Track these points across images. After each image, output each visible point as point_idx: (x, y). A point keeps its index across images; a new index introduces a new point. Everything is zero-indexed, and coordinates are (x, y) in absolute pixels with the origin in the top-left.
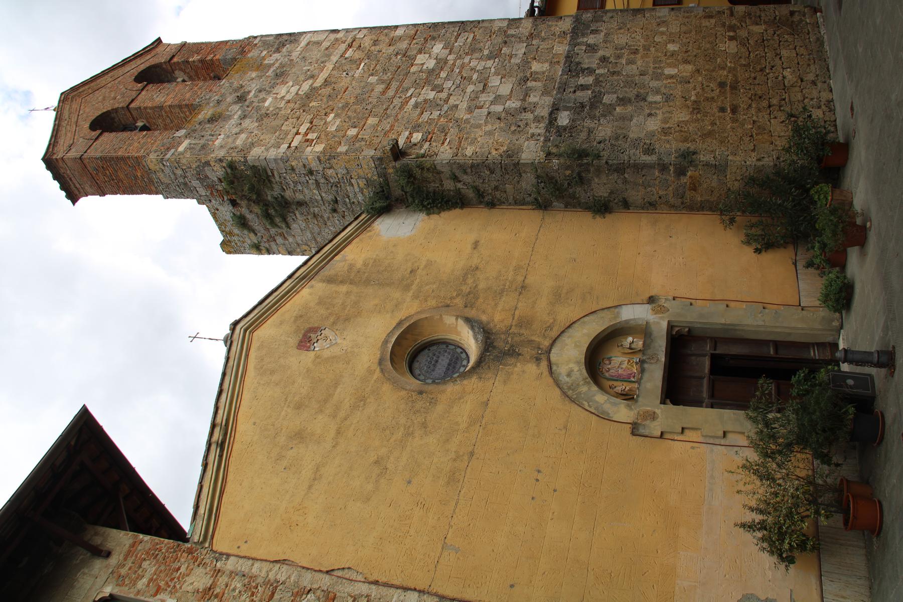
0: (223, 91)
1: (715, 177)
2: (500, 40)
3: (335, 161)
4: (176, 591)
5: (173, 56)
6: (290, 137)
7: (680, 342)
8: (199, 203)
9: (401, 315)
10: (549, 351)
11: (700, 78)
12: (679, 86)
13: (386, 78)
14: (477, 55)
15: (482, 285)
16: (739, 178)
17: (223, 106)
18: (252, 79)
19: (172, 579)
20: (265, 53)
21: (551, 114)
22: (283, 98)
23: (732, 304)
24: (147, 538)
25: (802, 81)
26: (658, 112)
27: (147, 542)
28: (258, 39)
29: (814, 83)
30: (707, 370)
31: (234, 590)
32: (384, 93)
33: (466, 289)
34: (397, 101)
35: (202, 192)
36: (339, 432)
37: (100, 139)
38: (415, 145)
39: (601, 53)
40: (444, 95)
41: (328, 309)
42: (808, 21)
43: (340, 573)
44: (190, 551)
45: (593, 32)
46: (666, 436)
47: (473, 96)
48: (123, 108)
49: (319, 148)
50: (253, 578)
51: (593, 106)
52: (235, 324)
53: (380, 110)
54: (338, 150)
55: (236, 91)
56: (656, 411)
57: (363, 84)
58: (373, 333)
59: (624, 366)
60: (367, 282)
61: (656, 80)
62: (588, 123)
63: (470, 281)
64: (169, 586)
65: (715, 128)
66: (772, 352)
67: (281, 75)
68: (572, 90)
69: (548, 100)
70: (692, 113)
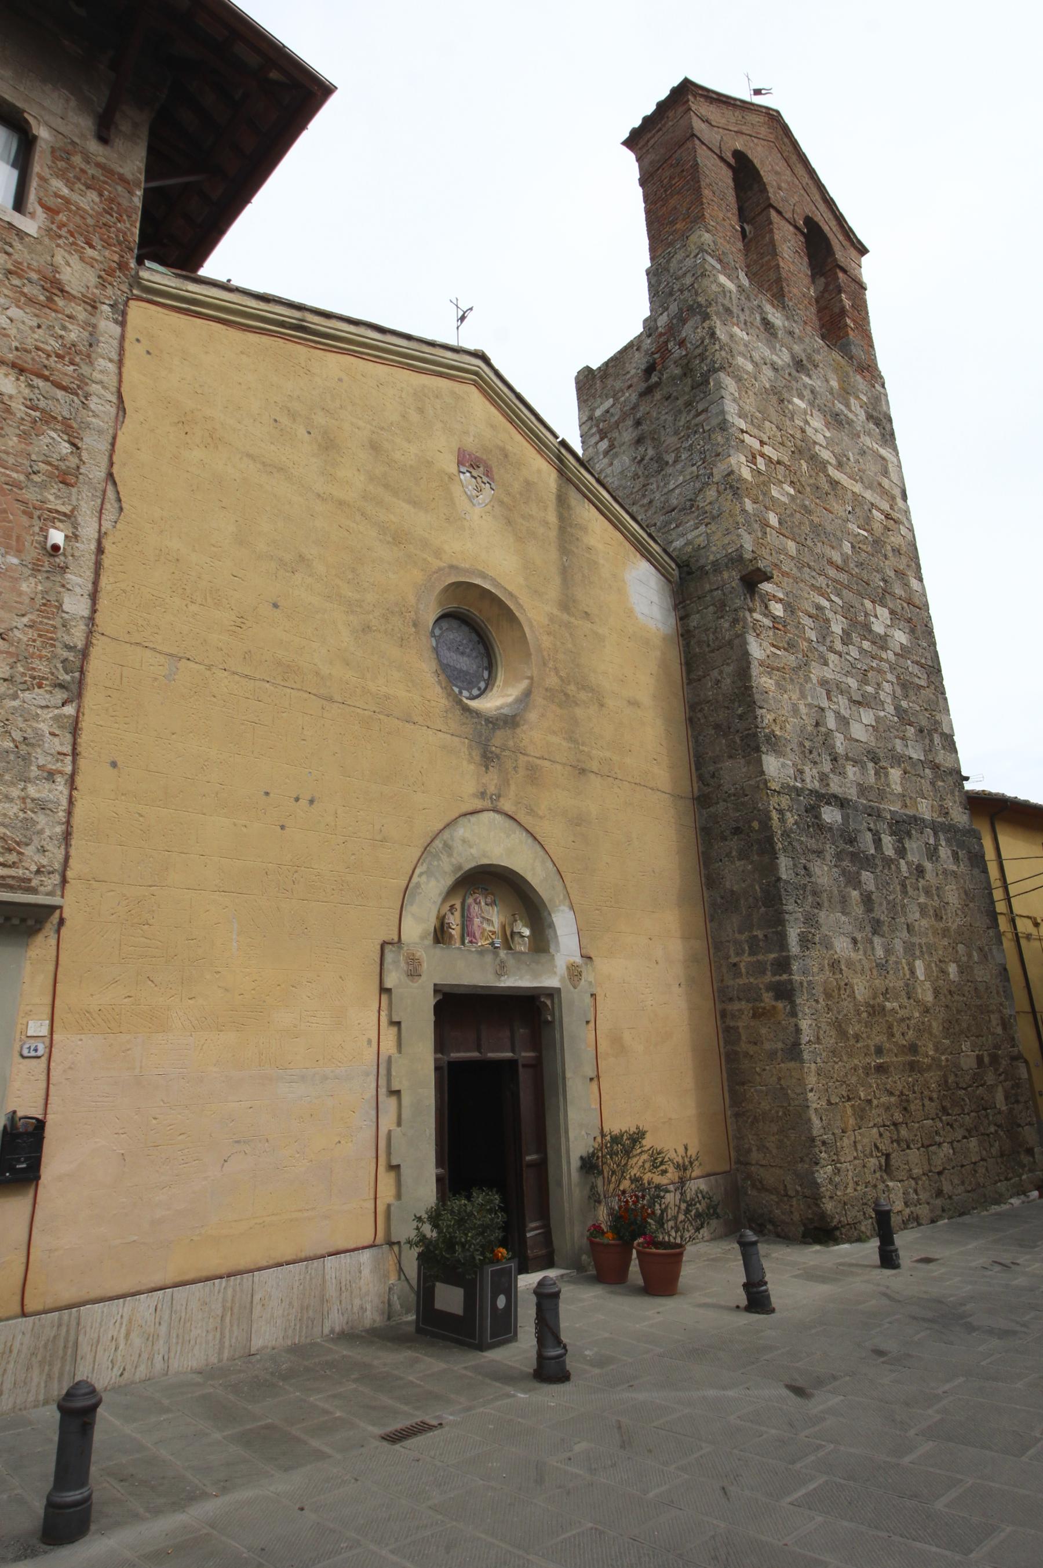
0: (807, 340)
1: (780, 1045)
2: (924, 723)
3: (730, 497)
4: (51, 238)
5: (845, 271)
6: (755, 431)
7: (530, 1013)
8: (645, 321)
9: (525, 599)
10: (495, 810)
11: (917, 1014)
12: (901, 983)
13: (852, 565)
14: (899, 691)
15: (579, 712)
16: (782, 1082)
17: (788, 340)
18: (827, 381)
20: (865, 399)
21: (835, 796)
22: (807, 422)
23: (595, 1082)
24: (137, 201)
25: (940, 1173)
26: (861, 952)
27: (131, 201)
28: (882, 390)
29: (939, 1193)
30: (491, 1055)
32: (831, 562)
33: (571, 689)
34: (821, 581)
35: (663, 320)
36: (341, 503)
37: (722, 164)
38: (766, 607)
39: (928, 866)
40: (838, 646)
41: (521, 494)
42: (1024, 1177)
43: (110, 494)
44: (122, 266)
45: (955, 855)
46: (384, 997)
47: (843, 686)
48: (768, 198)
49: (746, 473)
50: (89, 358)
51: (854, 856)
53: (807, 558)
54: (746, 500)
55: (809, 358)
56: (423, 978)
57: (839, 534)
58: (493, 554)
59: (485, 925)
60: (564, 549)
61: (905, 949)
62: (830, 850)
63: (583, 696)
64: (59, 228)
65: (852, 1042)
66: (528, 1158)
67: (836, 421)
68: (872, 826)
69: (852, 793)
70: (867, 1004)
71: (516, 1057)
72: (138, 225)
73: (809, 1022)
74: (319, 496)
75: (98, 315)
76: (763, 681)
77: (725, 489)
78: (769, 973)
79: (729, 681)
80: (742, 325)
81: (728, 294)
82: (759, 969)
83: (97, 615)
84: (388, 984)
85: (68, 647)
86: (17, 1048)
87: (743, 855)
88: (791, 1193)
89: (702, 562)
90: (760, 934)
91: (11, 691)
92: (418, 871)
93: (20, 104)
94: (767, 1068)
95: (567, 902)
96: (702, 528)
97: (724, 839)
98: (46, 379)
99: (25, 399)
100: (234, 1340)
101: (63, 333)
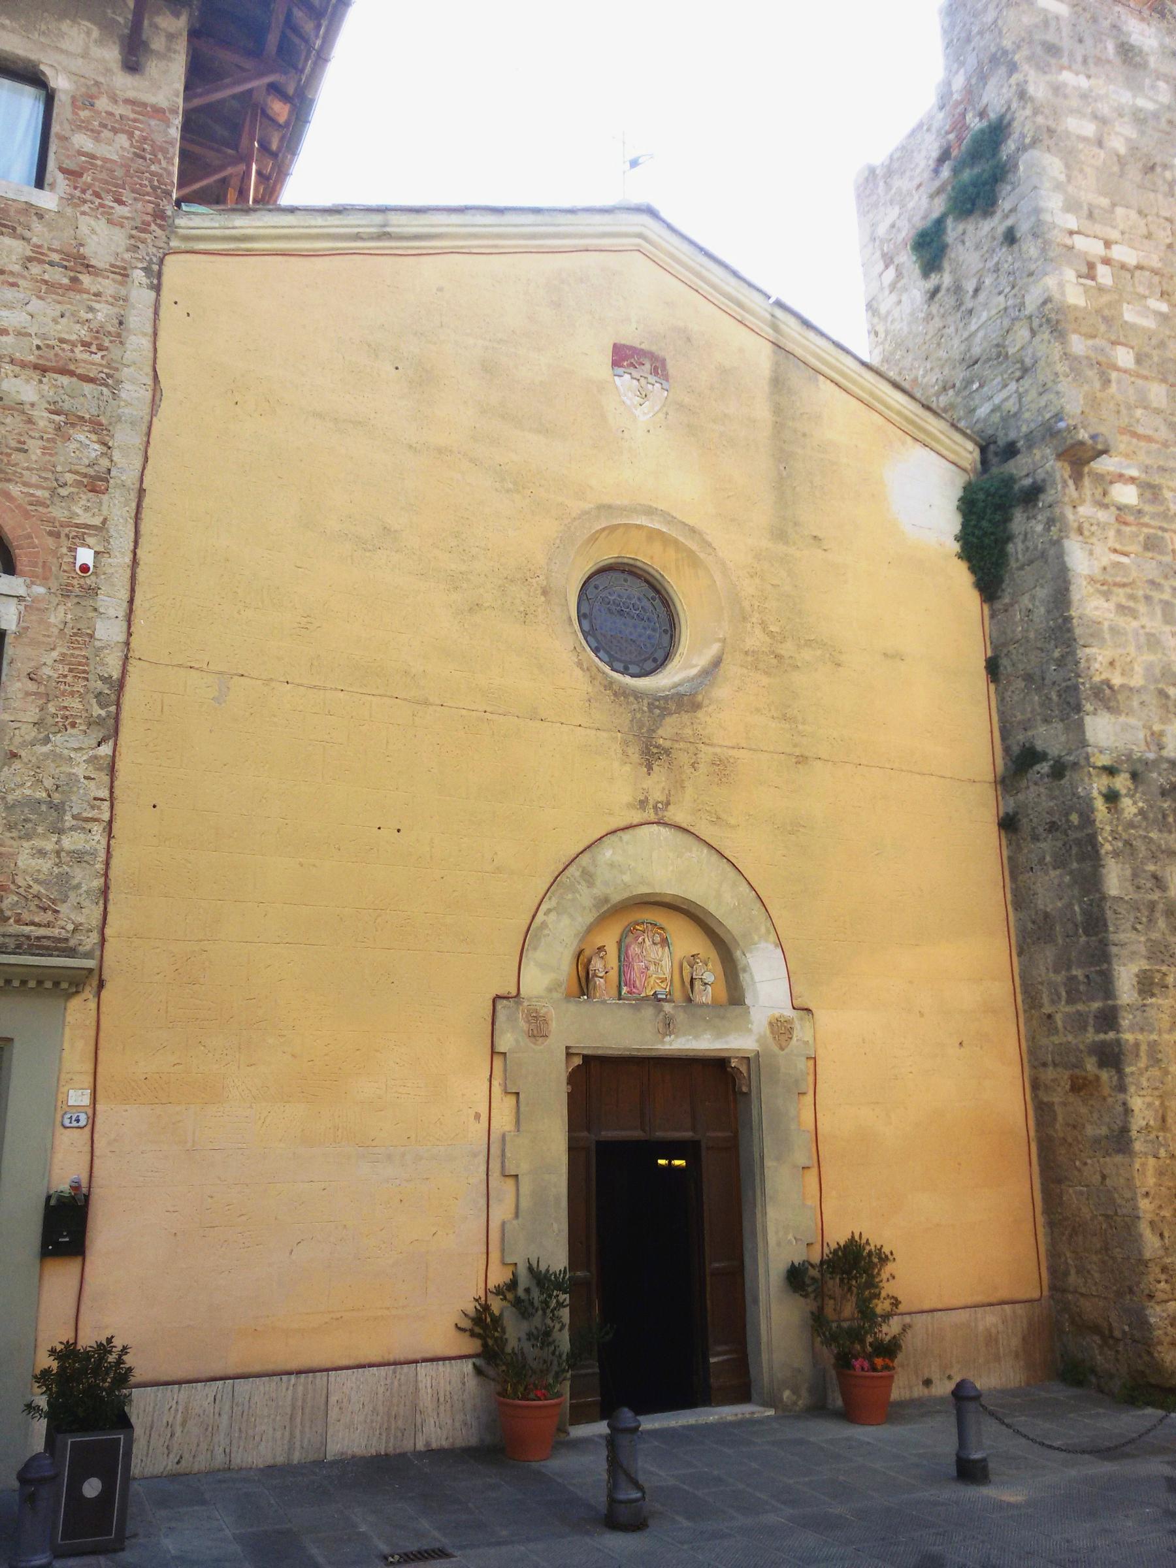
1: (1104, 1131)
3: (1046, 336)
16: (1108, 1181)
19: (98, 195)
24: (175, 133)
27: (167, 134)
31: (91, 309)
33: (787, 649)
35: (959, 82)
50: (119, 338)
52: (651, 212)
63: (807, 654)
71: (697, 1138)
72: (177, 161)
73: (1148, 1099)
74: (411, 447)
75: (130, 283)
76: (1090, 606)
77: (1041, 326)
78: (1091, 1029)
79: (1042, 610)
80: (1078, 66)
81: (1053, 23)
82: (1079, 1023)
83: (132, 639)
84: (501, 1048)
85: (103, 679)
86: (59, 1119)
87: (1060, 862)
88: (1117, 1334)
89: (1012, 435)
90: (1078, 972)
91: (41, 736)
92: (544, 907)
93: (33, 56)
94: (1089, 1161)
95: (773, 937)
96: (1013, 386)
97: (1036, 838)
98: (72, 374)
99: (49, 403)
100: (306, 1441)
101: (90, 316)
